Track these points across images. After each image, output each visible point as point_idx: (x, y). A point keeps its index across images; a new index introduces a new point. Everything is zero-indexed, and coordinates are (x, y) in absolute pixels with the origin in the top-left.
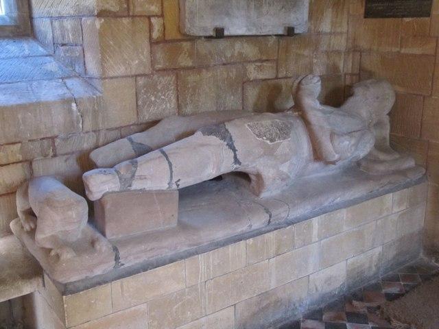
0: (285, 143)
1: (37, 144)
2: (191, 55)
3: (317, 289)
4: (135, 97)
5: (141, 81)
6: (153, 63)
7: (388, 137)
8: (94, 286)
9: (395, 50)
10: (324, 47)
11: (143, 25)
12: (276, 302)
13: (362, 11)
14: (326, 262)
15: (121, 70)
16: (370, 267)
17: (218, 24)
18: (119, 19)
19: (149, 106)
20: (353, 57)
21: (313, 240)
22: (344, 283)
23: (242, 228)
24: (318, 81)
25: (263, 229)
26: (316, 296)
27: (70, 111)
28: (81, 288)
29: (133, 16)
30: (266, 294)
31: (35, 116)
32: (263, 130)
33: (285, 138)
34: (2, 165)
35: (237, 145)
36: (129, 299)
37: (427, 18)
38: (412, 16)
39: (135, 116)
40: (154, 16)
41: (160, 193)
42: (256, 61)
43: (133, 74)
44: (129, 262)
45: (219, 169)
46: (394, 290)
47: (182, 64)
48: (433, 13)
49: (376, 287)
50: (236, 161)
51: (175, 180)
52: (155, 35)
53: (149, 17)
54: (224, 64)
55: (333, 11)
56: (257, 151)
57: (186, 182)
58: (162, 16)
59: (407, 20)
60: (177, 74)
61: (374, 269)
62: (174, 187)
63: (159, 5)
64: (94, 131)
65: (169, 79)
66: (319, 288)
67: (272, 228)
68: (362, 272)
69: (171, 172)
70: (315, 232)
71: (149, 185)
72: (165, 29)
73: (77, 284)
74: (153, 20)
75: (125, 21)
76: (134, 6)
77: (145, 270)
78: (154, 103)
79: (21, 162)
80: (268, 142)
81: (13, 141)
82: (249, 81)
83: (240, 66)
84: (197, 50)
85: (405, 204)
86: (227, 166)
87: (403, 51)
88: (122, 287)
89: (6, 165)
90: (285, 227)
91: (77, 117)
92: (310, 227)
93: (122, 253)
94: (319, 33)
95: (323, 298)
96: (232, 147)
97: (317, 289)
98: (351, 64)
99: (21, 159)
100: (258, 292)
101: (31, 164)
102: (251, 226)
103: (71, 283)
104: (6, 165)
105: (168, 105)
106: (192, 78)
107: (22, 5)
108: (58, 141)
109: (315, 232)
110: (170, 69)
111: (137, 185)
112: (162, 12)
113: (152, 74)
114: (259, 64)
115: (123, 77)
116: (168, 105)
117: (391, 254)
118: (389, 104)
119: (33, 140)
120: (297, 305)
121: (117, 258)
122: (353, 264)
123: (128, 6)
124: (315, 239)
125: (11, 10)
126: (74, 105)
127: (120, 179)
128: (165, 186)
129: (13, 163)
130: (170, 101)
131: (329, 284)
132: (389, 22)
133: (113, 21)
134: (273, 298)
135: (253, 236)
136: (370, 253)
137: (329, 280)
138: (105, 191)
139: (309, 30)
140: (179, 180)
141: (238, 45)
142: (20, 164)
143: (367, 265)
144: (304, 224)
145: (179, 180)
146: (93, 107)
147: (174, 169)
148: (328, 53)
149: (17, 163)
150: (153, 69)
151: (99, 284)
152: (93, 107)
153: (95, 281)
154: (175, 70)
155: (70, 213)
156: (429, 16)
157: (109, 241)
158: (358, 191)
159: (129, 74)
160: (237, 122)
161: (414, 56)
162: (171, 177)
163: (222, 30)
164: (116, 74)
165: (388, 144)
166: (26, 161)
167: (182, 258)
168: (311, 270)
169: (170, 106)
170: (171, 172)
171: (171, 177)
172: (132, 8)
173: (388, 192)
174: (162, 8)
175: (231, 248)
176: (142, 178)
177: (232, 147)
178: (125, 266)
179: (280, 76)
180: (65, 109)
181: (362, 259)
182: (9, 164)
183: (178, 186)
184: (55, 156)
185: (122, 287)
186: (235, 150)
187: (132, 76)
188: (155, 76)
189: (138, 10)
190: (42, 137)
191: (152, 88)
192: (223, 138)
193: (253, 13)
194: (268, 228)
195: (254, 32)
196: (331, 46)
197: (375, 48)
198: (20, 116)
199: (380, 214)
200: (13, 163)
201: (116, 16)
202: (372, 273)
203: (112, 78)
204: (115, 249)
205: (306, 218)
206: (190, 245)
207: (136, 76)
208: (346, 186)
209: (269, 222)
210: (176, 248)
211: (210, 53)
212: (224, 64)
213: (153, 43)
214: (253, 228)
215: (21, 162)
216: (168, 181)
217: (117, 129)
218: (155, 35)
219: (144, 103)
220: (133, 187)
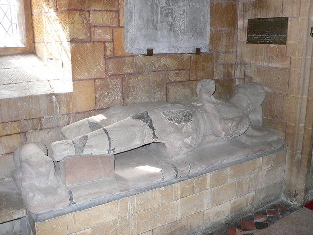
0: (189, 124)
1: (30, 122)
2: (132, 66)
3: (210, 220)
4: (94, 93)
5: (98, 83)
6: (106, 70)
7: (261, 120)
8: (55, 216)
9: (265, 64)
10: (221, 61)
11: (100, 47)
12: (181, 228)
13: (246, 39)
14: (216, 202)
15: (85, 75)
16: (247, 205)
17: (150, 47)
18: (84, 44)
19: (104, 98)
20: (240, 68)
21: (207, 188)
22: (229, 216)
23: (211, 145)
24: (214, 84)
25: (172, 181)
26: (209, 224)
27: (52, 101)
28: (47, 218)
29: (94, 42)
30: (175, 223)
31: (29, 105)
32: (173, 116)
33: (188, 122)
34: (1, 136)
35: (154, 126)
36: (80, 225)
37: (285, 45)
38: (275, 44)
39: (94, 105)
40: (107, 41)
41: (102, 157)
42: (175, 70)
43: (93, 78)
44: (80, 203)
45: (143, 141)
46: (261, 220)
47: (126, 72)
48: (288, 42)
49: (251, 219)
50: (154, 136)
51: (112, 148)
52: (108, 53)
53: (104, 43)
54: (154, 72)
55: (227, 39)
56: (169, 130)
57: (118, 151)
58: (113, 41)
59: (273, 45)
60: (122, 78)
61: (249, 206)
62: (112, 153)
63: (111, 35)
64: (67, 114)
65: (117, 81)
66: (211, 219)
67: (179, 180)
68: (242, 208)
69: (110, 143)
70: (208, 182)
71: (95, 152)
72: (114, 49)
73: (44, 215)
74: (107, 44)
75: (88, 45)
76: (94, 35)
77: (90, 207)
78: (107, 96)
79: (19, 133)
80: (176, 124)
81: (15, 120)
82: (170, 82)
83: (164, 73)
84: (136, 63)
85: (271, 164)
86: (148, 139)
87: (270, 65)
88: (74, 216)
89: (10, 135)
90: (187, 179)
91: (56, 105)
92: (205, 179)
93: (74, 195)
94: (217, 52)
95: (214, 226)
96: (151, 127)
97: (210, 220)
98: (239, 72)
99: (19, 131)
100: (168, 221)
101: (26, 135)
102: (163, 179)
103: (40, 214)
104: (10, 135)
105: (116, 98)
106: (132, 80)
107: (29, 34)
108: (43, 120)
109: (208, 182)
110: (117, 75)
111: (86, 152)
112: (113, 39)
113: (106, 78)
114: (177, 71)
115: (86, 80)
116: (116, 98)
117: (261, 196)
118: (261, 99)
119: (27, 120)
120: (196, 230)
121: (71, 199)
122: (235, 203)
123: (91, 35)
124: (208, 187)
125: (22, 38)
126: (54, 97)
127: (75, 147)
128: (105, 152)
129: (14, 134)
130: (118, 95)
131: (218, 217)
132: (261, 46)
133: (80, 45)
134: (179, 225)
135: (165, 185)
136: (247, 195)
137: (218, 214)
138: (65, 155)
139: (211, 50)
140: (115, 149)
141: (163, 60)
142: (19, 135)
143: (245, 204)
144: (201, 178)
145: (115, 149)
146: (67, 99)
147: (111, 141)
148: (224, 65)
149: (17, 134)
150: (107, 75)
151: (59, 215)
152: (67, 99)
153: (56, 213)
154: (120, 75)
155: (41, 169)
156: (285, 44)
157: (67, 188)
158: (238, 156)
159: (91, 78)
160: (156, 110)
161: (277, 68)
162: (110, 146)
163: (152, 50)
164: (82, 78)
165: (261, 124)
166: (23, 132)
167: (116, 199)
168: (205, 208)
169: (119, 98)
170: (110, 143)
171: (110, 146)
172: (93, 36)
173: (259, 156)
174: (113, 37)
175: (149, 193)
176: (90, 147)
177: (151, 127)
178: (77, 204)
179: (191, 79)
180: (47, 100)
181: (241, 199)
182: (12, 134)
183: (114, 152)
184: (41, 129)
185: (74, 216)
186: (153, 129)
187: (93, 79)
188: (108, 80)
189: (97, 38)
190: (33, 117)
191: (106, 87)
192: (146, 122)
193: (173, 40)
194: (176, 180)
195: (173, 52)
196: (226, 60)
197: (254, 62)
198: (19, 104)
199: (254, 170)
200: (14, 134)
201: (82, 41)
202: (247, 209)
203: (79, 80)
204: (70, 193)
205: (202, 174)
206: (121, 191)
207: (95, 79)
208: (230, 153)
209: (176, 176)
210: (111, 193)
211: (145, 64)
212: (154, 72)
213: (106, 58)
214: (165, 180)
215: (19, 133)
216: (108, 149)
217: (82, 112)
218: (108, 53)
219: (100, 96)
220: (84, 153)
